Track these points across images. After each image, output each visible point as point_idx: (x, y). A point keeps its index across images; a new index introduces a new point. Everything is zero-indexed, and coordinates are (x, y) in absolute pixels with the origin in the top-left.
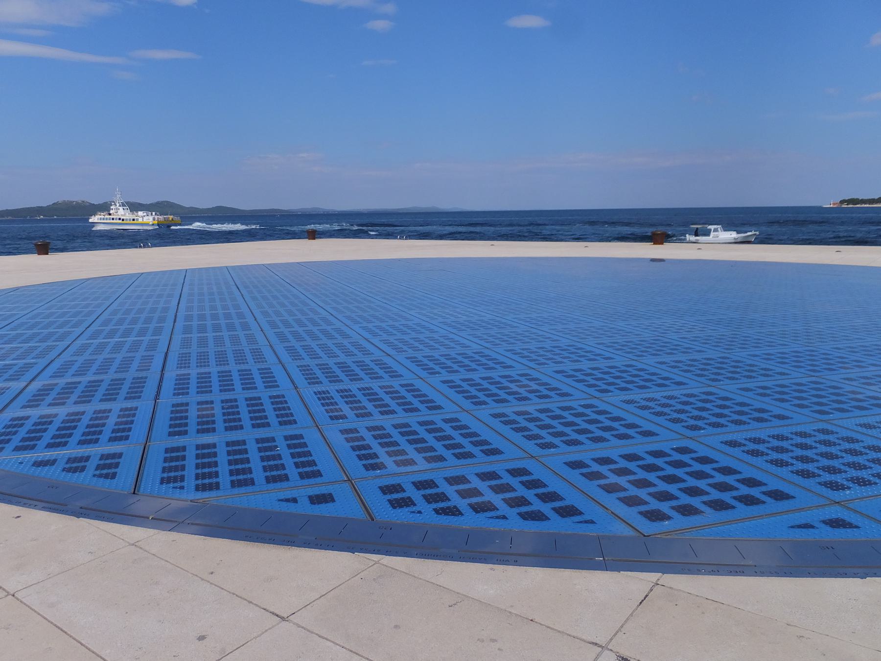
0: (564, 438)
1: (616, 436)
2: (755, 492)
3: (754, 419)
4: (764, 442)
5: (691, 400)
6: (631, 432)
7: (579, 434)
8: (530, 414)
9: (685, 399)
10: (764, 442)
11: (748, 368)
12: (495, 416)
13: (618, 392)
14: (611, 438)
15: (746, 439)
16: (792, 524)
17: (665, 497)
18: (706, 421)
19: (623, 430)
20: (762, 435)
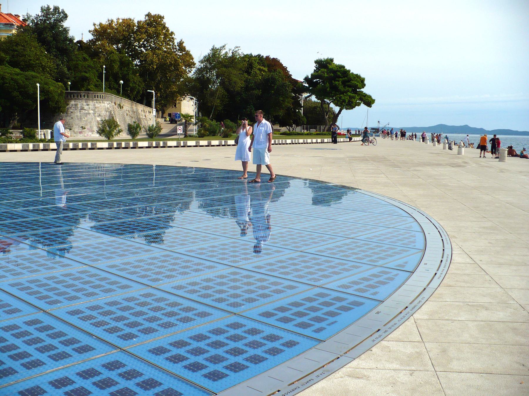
0: (84, 292)
1: (120, 287)
2: (190, 315)
3: (243, 259)
4: (226, 277)
5: (155, 261)
6: (113, 287)
7: (59, 296)
8: (56, 278)
9: (150, 261)
10: (226, 277)
11: (193, 237)
12: (12, 285)
13: (131, 255)
14: (83, 297)
15: (215, 277)
16: (336, 324)
17: (133, 325)
18: (190, 269)
19: (108, 287)
20: (198, 280)
